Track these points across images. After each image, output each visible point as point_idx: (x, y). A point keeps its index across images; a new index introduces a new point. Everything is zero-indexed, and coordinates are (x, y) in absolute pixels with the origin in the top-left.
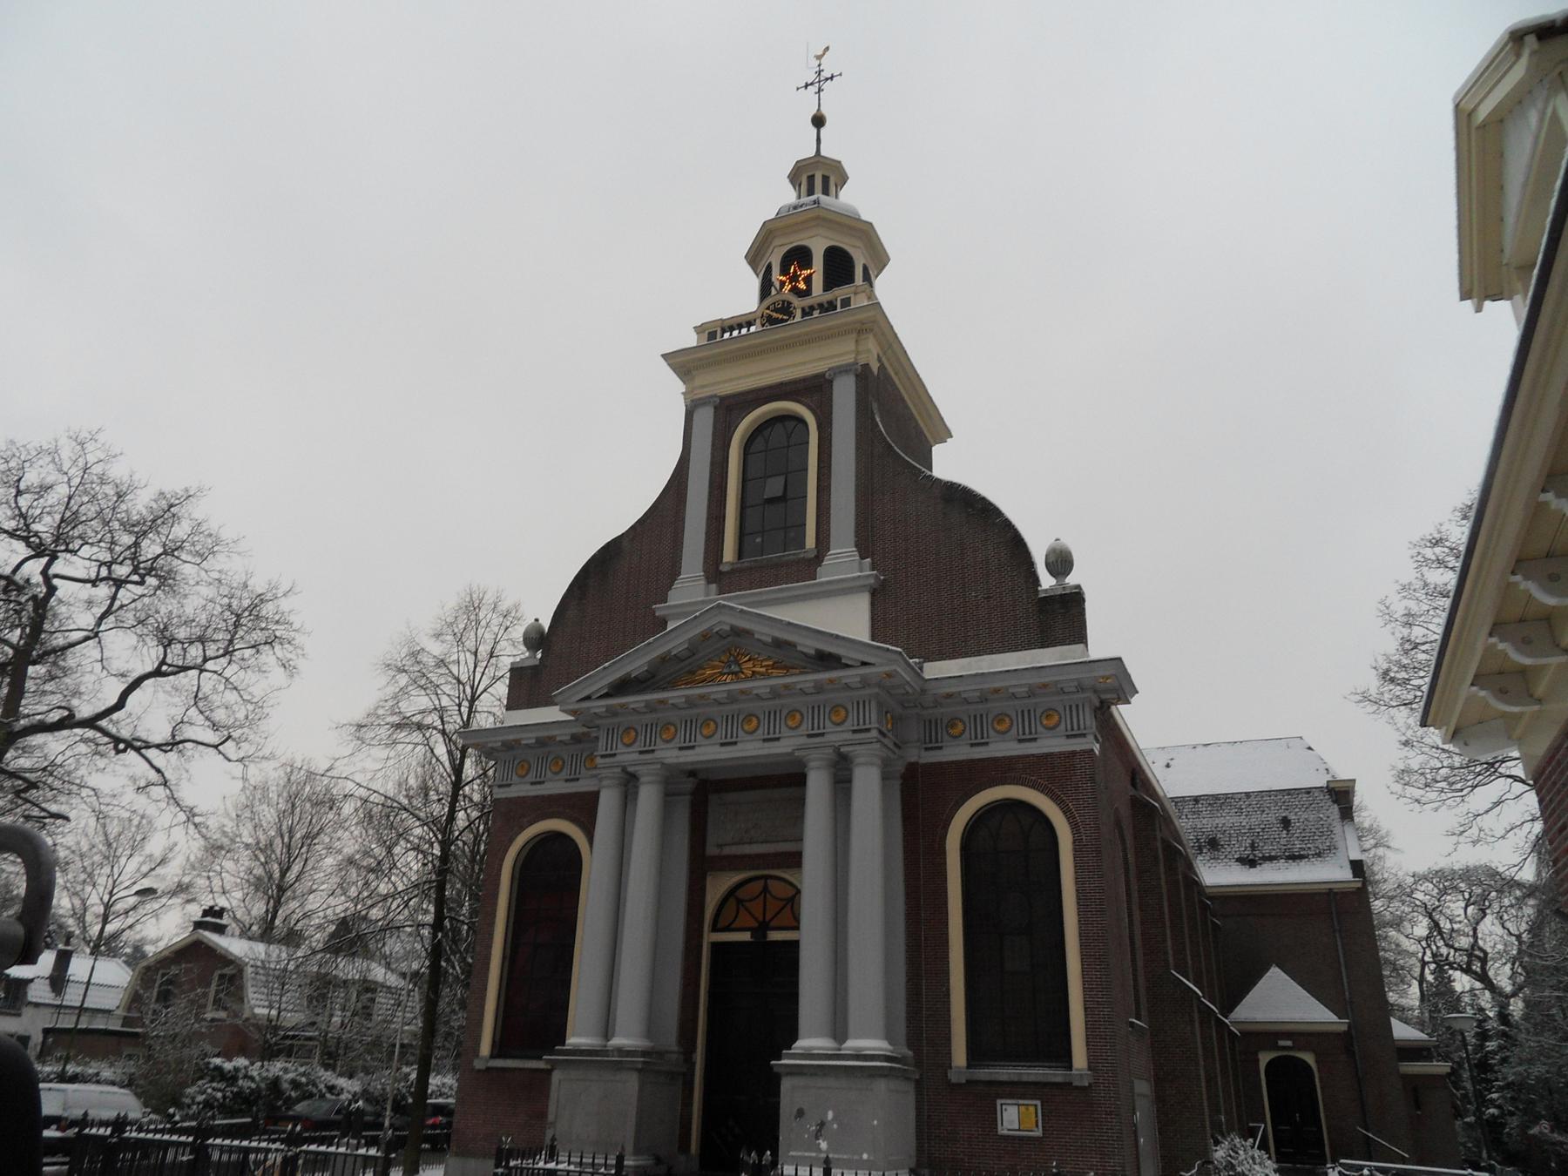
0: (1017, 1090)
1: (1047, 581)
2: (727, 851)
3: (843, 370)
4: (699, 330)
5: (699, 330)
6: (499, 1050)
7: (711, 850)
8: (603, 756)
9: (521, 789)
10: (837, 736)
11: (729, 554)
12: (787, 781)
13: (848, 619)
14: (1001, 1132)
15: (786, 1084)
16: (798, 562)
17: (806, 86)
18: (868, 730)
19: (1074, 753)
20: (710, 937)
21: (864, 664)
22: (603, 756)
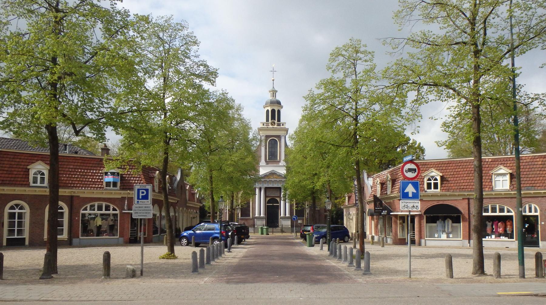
12: (280, 189)
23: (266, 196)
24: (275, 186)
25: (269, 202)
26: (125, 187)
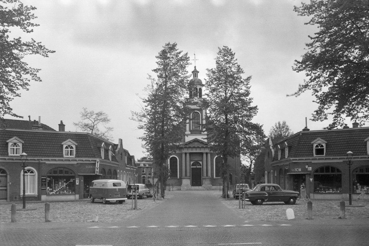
12: (202, 154)
23: (191, 161)
24: (198, 151)
25: (193, 165)
26: (79, 155)
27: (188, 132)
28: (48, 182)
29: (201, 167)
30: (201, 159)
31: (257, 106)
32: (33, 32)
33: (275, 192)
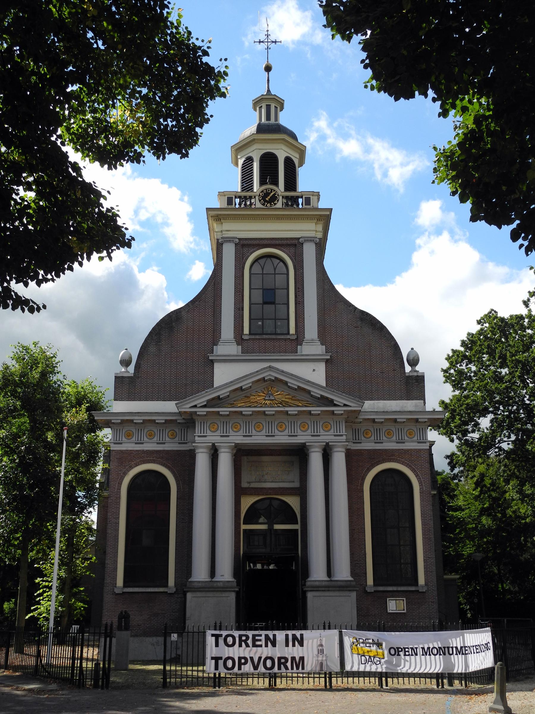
0: (394, 594)
1: (408, 369)
2: (253, 485)
3: (310, 240)
4: (221, 194)
5: (221, 194)
6: (126, 583)
7: (244, 485)
8: (199, 436)
9: (128, 446)
10: (327, 437)
11: (246, 331)
12: (299, 454)
13: (315, 374)
14: (389, 611)
15: (310, 595)
16: (285, 340)
17: (260, 42)
18: (342, 435)
19: (420, 450)
20: (243, 527)
21: (345, 405)
22: (199, 436)
23: (239, 491)
24: (282, 438)
25: (252, 515)
27: (227, 346)
28: (34, 615)
29: (297, 527)
30: (297, 484)
31: (349, 42)
32: (100, 167)
33: (55, 518)
